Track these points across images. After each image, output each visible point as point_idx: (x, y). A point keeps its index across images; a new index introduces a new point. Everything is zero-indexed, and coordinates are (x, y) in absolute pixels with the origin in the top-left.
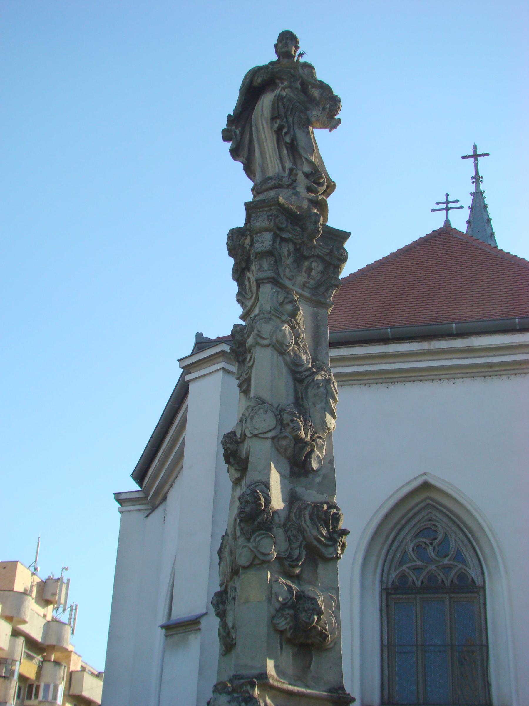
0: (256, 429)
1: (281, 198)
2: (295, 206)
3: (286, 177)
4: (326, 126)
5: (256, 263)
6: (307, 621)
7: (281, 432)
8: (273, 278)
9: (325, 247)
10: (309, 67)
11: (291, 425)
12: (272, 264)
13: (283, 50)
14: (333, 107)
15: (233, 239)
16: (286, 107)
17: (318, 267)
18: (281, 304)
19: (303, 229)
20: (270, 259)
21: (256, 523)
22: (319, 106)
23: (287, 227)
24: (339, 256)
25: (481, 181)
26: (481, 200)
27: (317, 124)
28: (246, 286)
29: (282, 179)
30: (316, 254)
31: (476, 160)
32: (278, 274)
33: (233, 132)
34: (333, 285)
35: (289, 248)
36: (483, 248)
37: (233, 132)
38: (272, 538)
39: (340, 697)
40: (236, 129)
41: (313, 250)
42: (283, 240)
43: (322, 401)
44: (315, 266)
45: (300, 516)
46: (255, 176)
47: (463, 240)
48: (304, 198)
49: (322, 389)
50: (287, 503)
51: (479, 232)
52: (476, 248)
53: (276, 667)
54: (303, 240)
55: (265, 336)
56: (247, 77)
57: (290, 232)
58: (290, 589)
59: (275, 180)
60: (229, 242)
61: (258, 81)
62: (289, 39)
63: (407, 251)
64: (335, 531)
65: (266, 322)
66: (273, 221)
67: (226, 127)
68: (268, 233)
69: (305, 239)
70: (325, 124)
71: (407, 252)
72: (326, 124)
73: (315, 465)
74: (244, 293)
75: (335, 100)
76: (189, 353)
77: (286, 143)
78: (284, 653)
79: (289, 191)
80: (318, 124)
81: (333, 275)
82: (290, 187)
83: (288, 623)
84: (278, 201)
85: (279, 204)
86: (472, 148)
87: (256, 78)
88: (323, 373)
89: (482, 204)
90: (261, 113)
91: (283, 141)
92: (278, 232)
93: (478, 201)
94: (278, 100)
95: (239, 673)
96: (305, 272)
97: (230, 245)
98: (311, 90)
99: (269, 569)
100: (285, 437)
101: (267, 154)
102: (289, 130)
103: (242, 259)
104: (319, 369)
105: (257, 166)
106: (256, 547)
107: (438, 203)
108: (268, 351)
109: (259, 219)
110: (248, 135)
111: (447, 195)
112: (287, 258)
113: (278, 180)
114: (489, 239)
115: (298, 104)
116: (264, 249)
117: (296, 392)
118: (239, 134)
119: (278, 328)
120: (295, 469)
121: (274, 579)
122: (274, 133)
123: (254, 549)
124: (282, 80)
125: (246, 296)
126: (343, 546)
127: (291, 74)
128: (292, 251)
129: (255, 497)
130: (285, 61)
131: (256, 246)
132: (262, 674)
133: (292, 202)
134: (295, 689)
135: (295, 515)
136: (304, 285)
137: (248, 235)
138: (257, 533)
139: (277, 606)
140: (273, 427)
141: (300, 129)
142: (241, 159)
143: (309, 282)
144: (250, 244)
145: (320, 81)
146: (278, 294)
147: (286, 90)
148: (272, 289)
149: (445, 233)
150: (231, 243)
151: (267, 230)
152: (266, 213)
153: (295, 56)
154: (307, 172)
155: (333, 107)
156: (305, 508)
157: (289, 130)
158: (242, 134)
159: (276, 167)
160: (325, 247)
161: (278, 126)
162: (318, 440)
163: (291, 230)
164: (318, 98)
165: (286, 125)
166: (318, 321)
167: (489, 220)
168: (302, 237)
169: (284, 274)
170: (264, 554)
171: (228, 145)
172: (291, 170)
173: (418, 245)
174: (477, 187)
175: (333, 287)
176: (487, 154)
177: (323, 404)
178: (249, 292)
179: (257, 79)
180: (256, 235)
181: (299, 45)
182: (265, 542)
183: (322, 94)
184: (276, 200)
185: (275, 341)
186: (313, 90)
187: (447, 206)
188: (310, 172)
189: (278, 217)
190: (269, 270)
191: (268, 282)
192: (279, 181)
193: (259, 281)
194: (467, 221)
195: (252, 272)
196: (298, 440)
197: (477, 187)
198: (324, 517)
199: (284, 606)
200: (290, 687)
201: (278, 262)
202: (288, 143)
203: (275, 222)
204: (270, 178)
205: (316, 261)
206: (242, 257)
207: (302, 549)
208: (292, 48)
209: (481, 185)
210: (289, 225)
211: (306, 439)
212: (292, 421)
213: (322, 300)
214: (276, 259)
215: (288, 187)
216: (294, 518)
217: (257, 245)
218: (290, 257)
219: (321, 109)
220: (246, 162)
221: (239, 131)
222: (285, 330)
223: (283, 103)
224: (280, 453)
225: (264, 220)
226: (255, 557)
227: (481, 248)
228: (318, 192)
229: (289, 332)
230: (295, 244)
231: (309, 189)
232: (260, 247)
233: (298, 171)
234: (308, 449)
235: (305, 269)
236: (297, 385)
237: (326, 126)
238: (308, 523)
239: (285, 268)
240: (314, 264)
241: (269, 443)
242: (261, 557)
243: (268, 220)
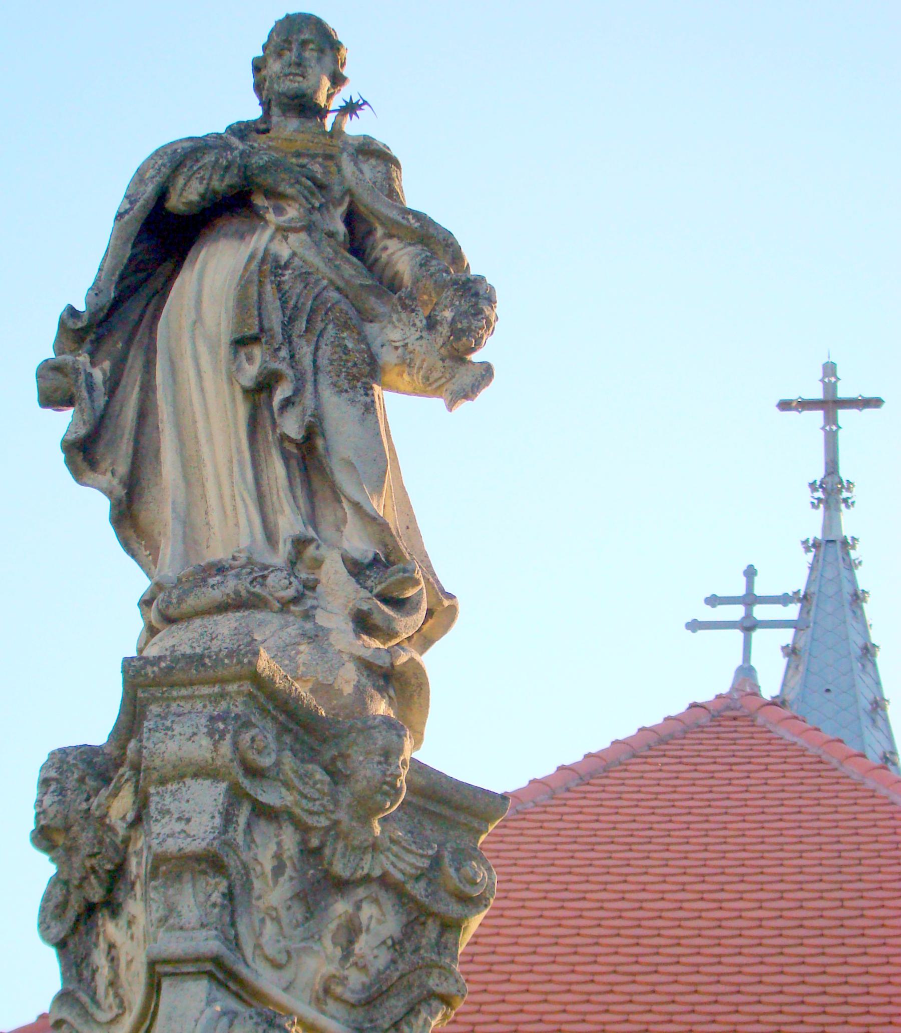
1: (264, 655)
2: (308, 681)
3: (281, 570)
4: (434, 386)
5: (153, 895)
8: (217, 960)
9: (413, 847)
12: (214, 905)
13: (289, 85)
14: (465, 321)
15: (62, 792)
16: (292, 303)
17: (380, 922)
19: (336, 776)
20: (207, 884)
22: (413, 311)
23: (278, 764)
24: (461, 886)
25: (845, 501)
26: (845, 573)
27: (401, 375)
28: (94, 972)
29: (264, 577)
30: (377, 873)
31: (831, 419)
32: (236, 944)
33: (82, 378)
34: (432, 995)
35: (279, 844)
36: (883, 792)
37: (82, 378)
40: (93, 364)
41: (368, 857)
42: (262, 811)
44: (371, 917)
46: (154, 550)
47: (807, 750)
48: (346, 657)
51: (828, 690)
52: (856, 787)
54: (334, 817)
56: (148, 175)
57: (287, 785)
59: (238, 576)
60: (48, 800)
62: (311, 46)
63: (592, 777)
67: (52, 355)
68: (208, 783)
69: (342, 815)
70: (431, 380)
71: (592, 781)
72: (436, 381)
74: (85, 998)
75: (477, 294)
77: (284, 438)
79: (287, 625)
80: (405, 376)
81: (434, 957)
82: (293, 608)
85: (257, 679)
86: (820, 376)
87: (181, 181)
89: (847, 589)
90: (193, 316)
91: (274, 431)
92: (245, 783)
93: (829, 573)
94: (260, 271)
96: (335, 943)
97: (51, 812)
98: (380, 246)
101: (208, 471)
102: (297, 391)
103: (93, 870)
105: (168, 514)
107: (713, 601)
109: (178, 729)
110: (137, 389)
111: (750, 573)
112: (271, 883)
113: (250, 578)
114: (865, 720)
115: (334, 295)
118: (105, 383)
122: (239, 396)
125: (93, 1009)
128: (291, 858)
131: (156, 828)
133: (298, 667)
136: (327, 991)
137: (127, 780)
142: (106, 479)
143: (346, 978)
144: (130, 816)
145: (419, 216)
146: (231, 1025)
147: (292, 237)
149: (735, 719)
150: (55, 808)
151: (205, 772)
152: (205, 706)
153: (328, 112)
154: (357, 555)
155: (465, 321)
157: (297, 391)
158: (114, 384)
159: (242, 526)
160: (413, 847)
161: (260, 374)
163: (291, 775)
164: (407, 279)
165: (290, 373)
167: (868, 651)
168: (331, 807)
172: (300, 544)
173: (634, 756)
174: (831, 521)
175: (435, 1003)
176: (876, 403)
178: (107, 995)
179: (185, 185)
180: (160, 789)
181: (345, 72)
183: (424, 264)
184: (246, 660)
186: (393, 245)
187: (748, 615)
188: (371, 556)
190: (203, 926)
191: (200, 974)
192: (251, 583)
193: (159, 969)
194: (784, 648)
195: (130, 924)
197: (831, 521)
202: (291, 440)
203: (235, 744)
204: (220, 569)
205: (376, 901)
206: (94, 861)
208: (319, 81)
209: (846, 516)
210: (288, 761)
214: (230, 888)
215: (285, 606)
217: (163, 827)
218: (281, 880)
219: (421, 322)
220: (123, 492)
221: (104, 374)
223: (279, 286)
225: (195, 734)
227: (874, 791)
228: (395, 634)
230: (303, 829)
232: (171, 835)
233: (323, 551)
235: (333, 926)
237: (434, 386)
239: (263, 921)
240: (368, 911)
243: (211, 734)
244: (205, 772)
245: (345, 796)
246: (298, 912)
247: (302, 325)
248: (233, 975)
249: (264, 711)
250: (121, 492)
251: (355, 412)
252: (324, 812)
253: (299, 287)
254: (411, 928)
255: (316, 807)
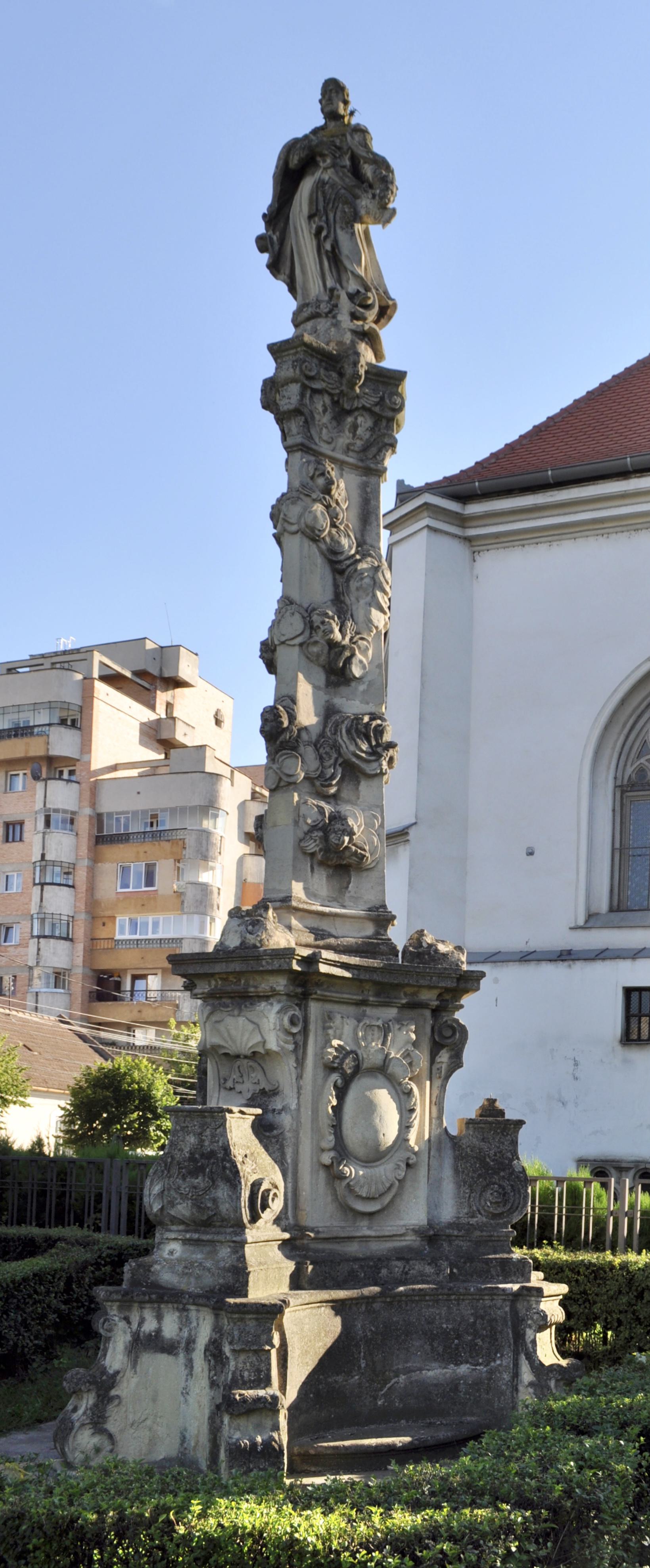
0: (284, 635)
6: (337, 842)
7: (311, 637)
8: (302, 445)
10: (361, 131)
11: (322, 628)
18: (312, 478)
19: (341, 374)
21: (278, 742)
23: (318, 373)
30: (360, 405)
32: (311, 438)
38: (297, 758)
39: (379, 916)
42: (315, 391)
43: (367, 595)
45: (336, 731)
49: (367, 580)
50: (322, 718)
53: (306, 889)
55: (292, 521)
58: (321, 811)
61: (294, 161)
64: (378, 745)
65: (293, 503)
66: (298, 368)
69: (344, 388)
73: (357, 671)
76: (392, 506)
77: (327, 252)
78: (316, 875)
83: (317, 845)
84: (302, 340)
85: (305, 344)
88: (369, 559)
92: (306, 382)
95: (267, 896)
96: (349, 432)
99: (295, 791)
100: (316, 643)
102: (329, 232)
104: (365, 555)
106: (280, 769)
108: (297, 538)
115: (343, 191)
116: (291, 407)
117: (336, 585)
119: (306, 509)
120: (333, 678)
121: (302, 801)
123: (278, 771)
124: (323, 156)
126: (391, 761)
127: (336, 146)
129: (275, 715)
130: (332, 124)
132: (288, 897)
134: (327, 910)
135: (330, 731)
136: (348, 449)
138: (280, 753)
139: (306, 828)
140: (300, 632)
141: (342, 229)
142: (282, 276)
147: (329, 171)
148: (301, 459)
151: (294, 380)
156: (343, 722)
157: (329, 232)
162: (360, 642)
166: (367, 493)
169: (320, 438)
170: (290, 776)
171: (266, 256)
177: (369, 599)
182: (289, 762)
185: (303, 526)
189: (305, 361)
190: (299, 434)
191: (297, 451)
196: (332, 645)
198: (363, 730)
199: (314, 828)
200: (321, 909)
201: (308, 423)
205: (362, 415)
207: (338, 766)
210: (322, 371)
211: (344, 643)
212: (323, 623)
213: (372, 466)
216: (329, 734)
219: (370, 196)
222: (316, 510)
223: (324, 193)
224: (312, 661)
226: (280, 779)
229: (322, 512)
230: (330, 394)
231: (354, 316)
234: (347, 654)
235: (348, 426)
236: (337, 576)
238: (345, 738)
239: (322, 429)
240: (360, 420)
241: (297, 649)
242: (285, 779)
244: (294, 380)
245: (344, 381)
246: (334, 423)
247: (331, 205)
248: (311, 449)
249: (312, 356)
250: (288, 281)
251: (347, 236)
252: (337, 388)
253: (330, 190)
254: (376, 424)
255: (334, 386)
